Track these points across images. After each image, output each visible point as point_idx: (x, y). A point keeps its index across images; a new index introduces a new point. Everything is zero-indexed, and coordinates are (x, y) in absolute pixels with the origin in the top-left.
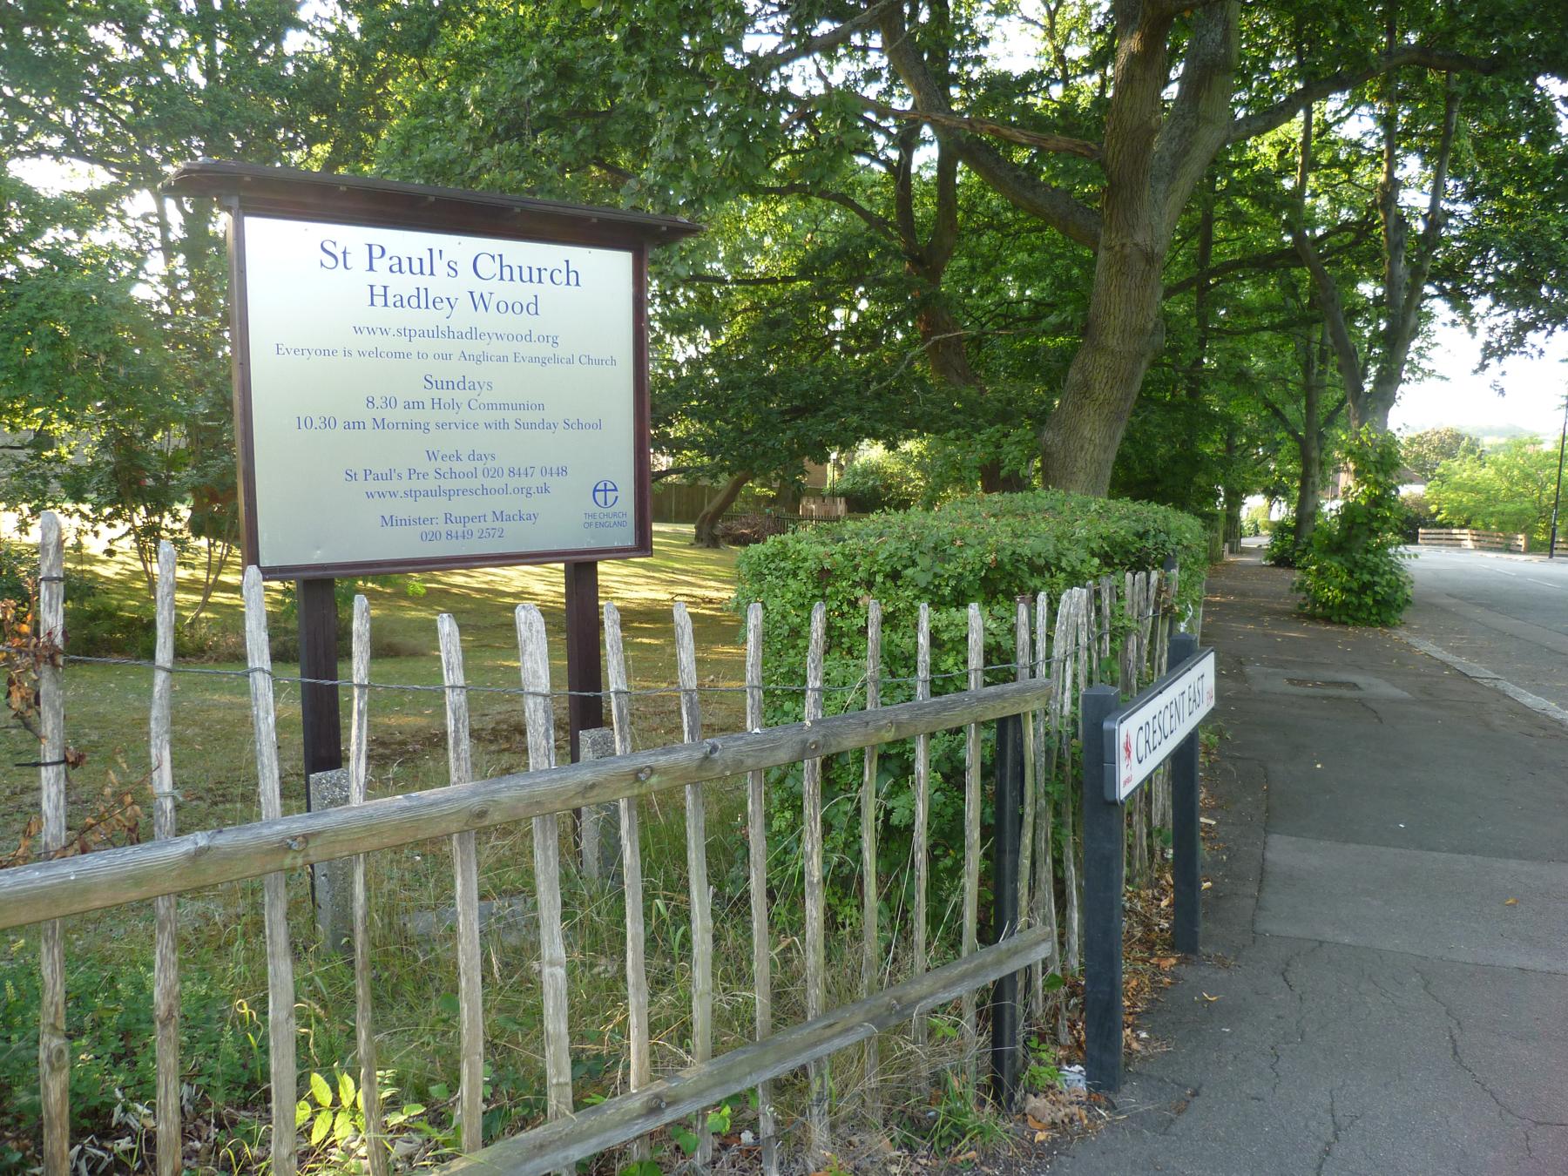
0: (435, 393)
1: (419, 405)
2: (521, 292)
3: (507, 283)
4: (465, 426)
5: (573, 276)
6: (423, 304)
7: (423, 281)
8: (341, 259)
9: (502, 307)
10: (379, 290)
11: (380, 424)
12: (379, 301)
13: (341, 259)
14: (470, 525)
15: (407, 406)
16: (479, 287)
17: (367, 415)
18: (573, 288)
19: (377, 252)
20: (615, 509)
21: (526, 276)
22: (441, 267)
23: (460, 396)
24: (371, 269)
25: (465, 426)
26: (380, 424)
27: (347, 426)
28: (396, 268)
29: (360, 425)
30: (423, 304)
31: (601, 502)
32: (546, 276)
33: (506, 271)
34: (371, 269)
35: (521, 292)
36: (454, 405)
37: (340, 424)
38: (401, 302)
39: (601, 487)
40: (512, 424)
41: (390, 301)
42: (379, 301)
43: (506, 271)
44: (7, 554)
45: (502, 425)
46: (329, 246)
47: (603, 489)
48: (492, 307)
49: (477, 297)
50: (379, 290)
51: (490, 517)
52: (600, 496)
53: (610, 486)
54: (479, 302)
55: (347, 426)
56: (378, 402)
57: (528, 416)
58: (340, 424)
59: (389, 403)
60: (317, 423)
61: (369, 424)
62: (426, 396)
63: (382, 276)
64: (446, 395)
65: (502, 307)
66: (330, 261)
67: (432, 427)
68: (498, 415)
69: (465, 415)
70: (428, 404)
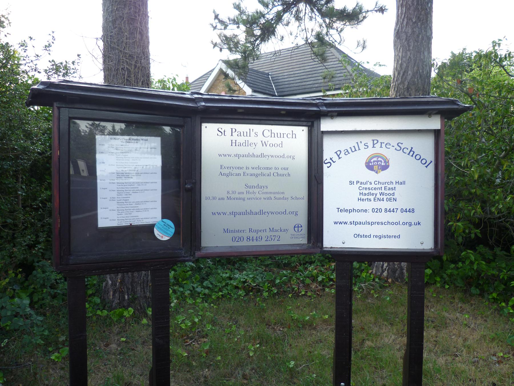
0: (248, 189)
1: (243, 193)
2: (277, 141)
3: (273, 138)
4: (257, 199)
5: (294, 135)
6: (247, 145)
7: (247, 138)
8: (223, 133)
9: (271, 145)
10: (234, 141)
11: (229, 198)
12: (234, 144)
13: (223, 133)
14: (260, 234)
15: (239, 193)
16: (264, 140)
17: (225, 196)
18: (294, 139)
19: (234, 130)
20: (301, 233)
21: (279, 136)
22: (252, 134)
23: (256, 190)
24: (232, 135)
25: (257, 199)
26: (229, 198)
27: (219, 199)
28: (239, 135)
29: (223, 199)
30: (247, 145)
31: (297, 231)
32: (285, 136)
33: (273, 135)
34: (232, 135)
35: (277, 141)
36: (254, 193)
37: (217, 199)
38: (240, 145)
39: (297, 226)
40: (273, 198)
41: (237, 145)
42: (234, 144)
43: (273, 135)
44: (507, 293)
45: (268, 199)
46: (220, 130)
47: (297, 227)
48: (268, 145)
49: (263, 142)
50: (234, 141)
51: (268, 230)
52: (296, 229)
53: (300, 226)
54: (264, 144)
55: (219, 199)
56: (230, 192)
57: (277, 196)
58: (217, 199)
59: (234, 192)
60: (211, 198)
61: (226, 198)
62: (244, 190)
63: (235, 137)
64: (251, 190)
65: (271, 145)
66: (220, 134)
67: (246, 199)
68: (268, 196)
69: (257, 195)
70: (245, 193)
